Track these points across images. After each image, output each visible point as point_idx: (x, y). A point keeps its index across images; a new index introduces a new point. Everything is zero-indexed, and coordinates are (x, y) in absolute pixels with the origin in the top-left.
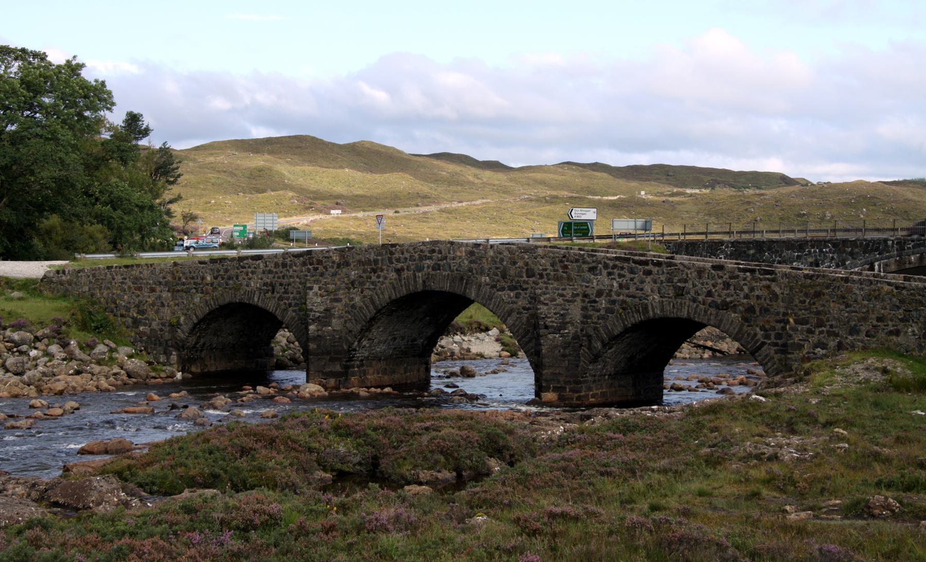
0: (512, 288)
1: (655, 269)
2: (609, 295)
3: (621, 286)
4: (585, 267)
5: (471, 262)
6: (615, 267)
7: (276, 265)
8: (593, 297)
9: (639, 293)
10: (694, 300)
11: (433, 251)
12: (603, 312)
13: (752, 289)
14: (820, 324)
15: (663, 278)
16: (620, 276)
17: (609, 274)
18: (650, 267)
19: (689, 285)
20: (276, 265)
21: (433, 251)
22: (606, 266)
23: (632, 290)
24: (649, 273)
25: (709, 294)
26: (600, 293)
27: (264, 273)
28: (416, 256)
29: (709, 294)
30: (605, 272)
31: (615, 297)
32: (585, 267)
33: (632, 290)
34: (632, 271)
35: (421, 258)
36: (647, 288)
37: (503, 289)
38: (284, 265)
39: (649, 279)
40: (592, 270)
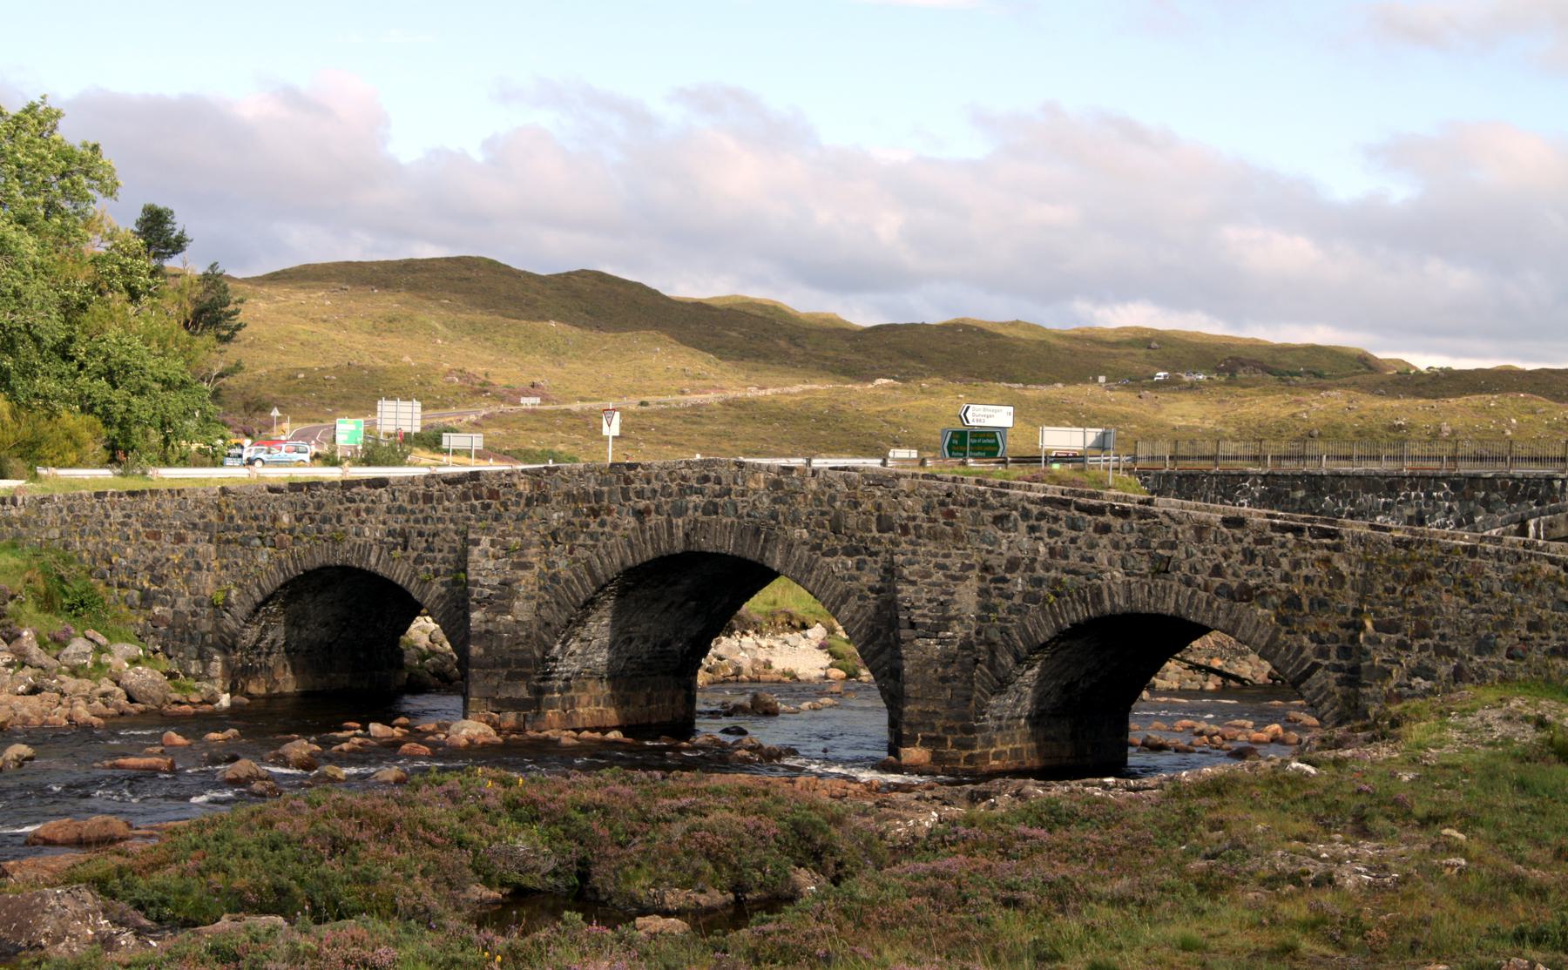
0: (849, 552)
1: (1117, 523)
2: (1030, 568)
3: (1052, 552)
4: (987, 515)
5: (775, 501)
6: (1042, 516)
7: (413, 497)
8: (1000, 572)
9: (1088, 566)
10: (1188, 582)
11: (706, 479)
12: (1017, 600)
13: (1296, 565)
14: (1422, 632)
15: (1131, 539)
16: (1053, 533)
17: (1032, 529)
18: (1108, 518)
19: (1180, 554)
20: (413, 497)
21: (706, 479)
22: (1026, 515)
23: (1074, 559)
24: (1105, 529)
25: (1217, 571)
26: (1013, 565)
27: (389, 511)
28: (674, 487)
29: (1217, 571)
30: (1023, 526)
31: (1041, 573)
32: (987, 515)
33: (1074, 559)
34: (1073, 526)
35: (682, 492)
36: (1102, 557)
37: (832, 552)
38: (428, 498)
39: (1104, 540)
40: (999, 520)
